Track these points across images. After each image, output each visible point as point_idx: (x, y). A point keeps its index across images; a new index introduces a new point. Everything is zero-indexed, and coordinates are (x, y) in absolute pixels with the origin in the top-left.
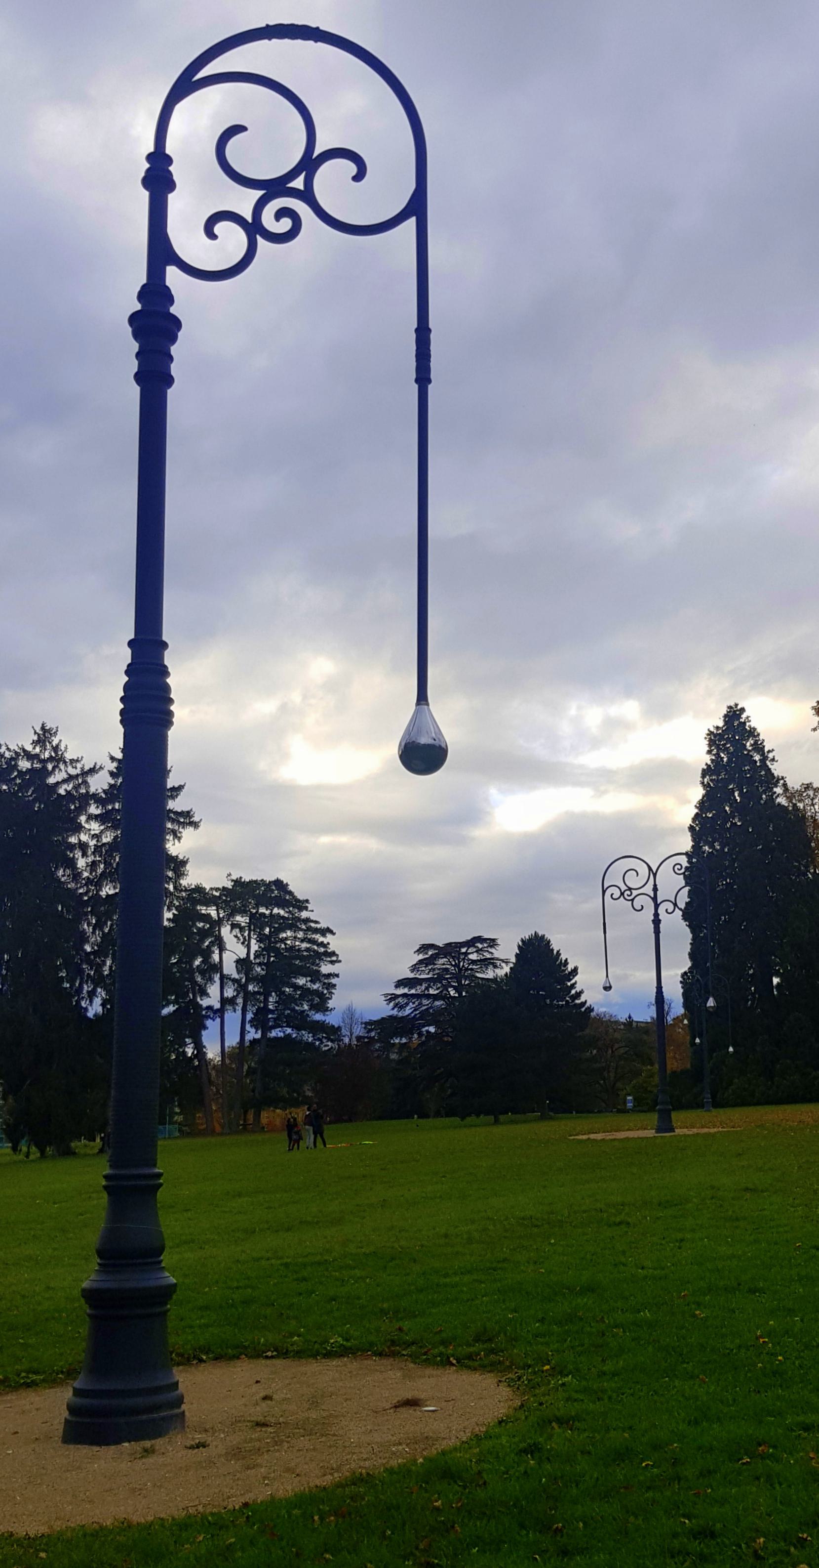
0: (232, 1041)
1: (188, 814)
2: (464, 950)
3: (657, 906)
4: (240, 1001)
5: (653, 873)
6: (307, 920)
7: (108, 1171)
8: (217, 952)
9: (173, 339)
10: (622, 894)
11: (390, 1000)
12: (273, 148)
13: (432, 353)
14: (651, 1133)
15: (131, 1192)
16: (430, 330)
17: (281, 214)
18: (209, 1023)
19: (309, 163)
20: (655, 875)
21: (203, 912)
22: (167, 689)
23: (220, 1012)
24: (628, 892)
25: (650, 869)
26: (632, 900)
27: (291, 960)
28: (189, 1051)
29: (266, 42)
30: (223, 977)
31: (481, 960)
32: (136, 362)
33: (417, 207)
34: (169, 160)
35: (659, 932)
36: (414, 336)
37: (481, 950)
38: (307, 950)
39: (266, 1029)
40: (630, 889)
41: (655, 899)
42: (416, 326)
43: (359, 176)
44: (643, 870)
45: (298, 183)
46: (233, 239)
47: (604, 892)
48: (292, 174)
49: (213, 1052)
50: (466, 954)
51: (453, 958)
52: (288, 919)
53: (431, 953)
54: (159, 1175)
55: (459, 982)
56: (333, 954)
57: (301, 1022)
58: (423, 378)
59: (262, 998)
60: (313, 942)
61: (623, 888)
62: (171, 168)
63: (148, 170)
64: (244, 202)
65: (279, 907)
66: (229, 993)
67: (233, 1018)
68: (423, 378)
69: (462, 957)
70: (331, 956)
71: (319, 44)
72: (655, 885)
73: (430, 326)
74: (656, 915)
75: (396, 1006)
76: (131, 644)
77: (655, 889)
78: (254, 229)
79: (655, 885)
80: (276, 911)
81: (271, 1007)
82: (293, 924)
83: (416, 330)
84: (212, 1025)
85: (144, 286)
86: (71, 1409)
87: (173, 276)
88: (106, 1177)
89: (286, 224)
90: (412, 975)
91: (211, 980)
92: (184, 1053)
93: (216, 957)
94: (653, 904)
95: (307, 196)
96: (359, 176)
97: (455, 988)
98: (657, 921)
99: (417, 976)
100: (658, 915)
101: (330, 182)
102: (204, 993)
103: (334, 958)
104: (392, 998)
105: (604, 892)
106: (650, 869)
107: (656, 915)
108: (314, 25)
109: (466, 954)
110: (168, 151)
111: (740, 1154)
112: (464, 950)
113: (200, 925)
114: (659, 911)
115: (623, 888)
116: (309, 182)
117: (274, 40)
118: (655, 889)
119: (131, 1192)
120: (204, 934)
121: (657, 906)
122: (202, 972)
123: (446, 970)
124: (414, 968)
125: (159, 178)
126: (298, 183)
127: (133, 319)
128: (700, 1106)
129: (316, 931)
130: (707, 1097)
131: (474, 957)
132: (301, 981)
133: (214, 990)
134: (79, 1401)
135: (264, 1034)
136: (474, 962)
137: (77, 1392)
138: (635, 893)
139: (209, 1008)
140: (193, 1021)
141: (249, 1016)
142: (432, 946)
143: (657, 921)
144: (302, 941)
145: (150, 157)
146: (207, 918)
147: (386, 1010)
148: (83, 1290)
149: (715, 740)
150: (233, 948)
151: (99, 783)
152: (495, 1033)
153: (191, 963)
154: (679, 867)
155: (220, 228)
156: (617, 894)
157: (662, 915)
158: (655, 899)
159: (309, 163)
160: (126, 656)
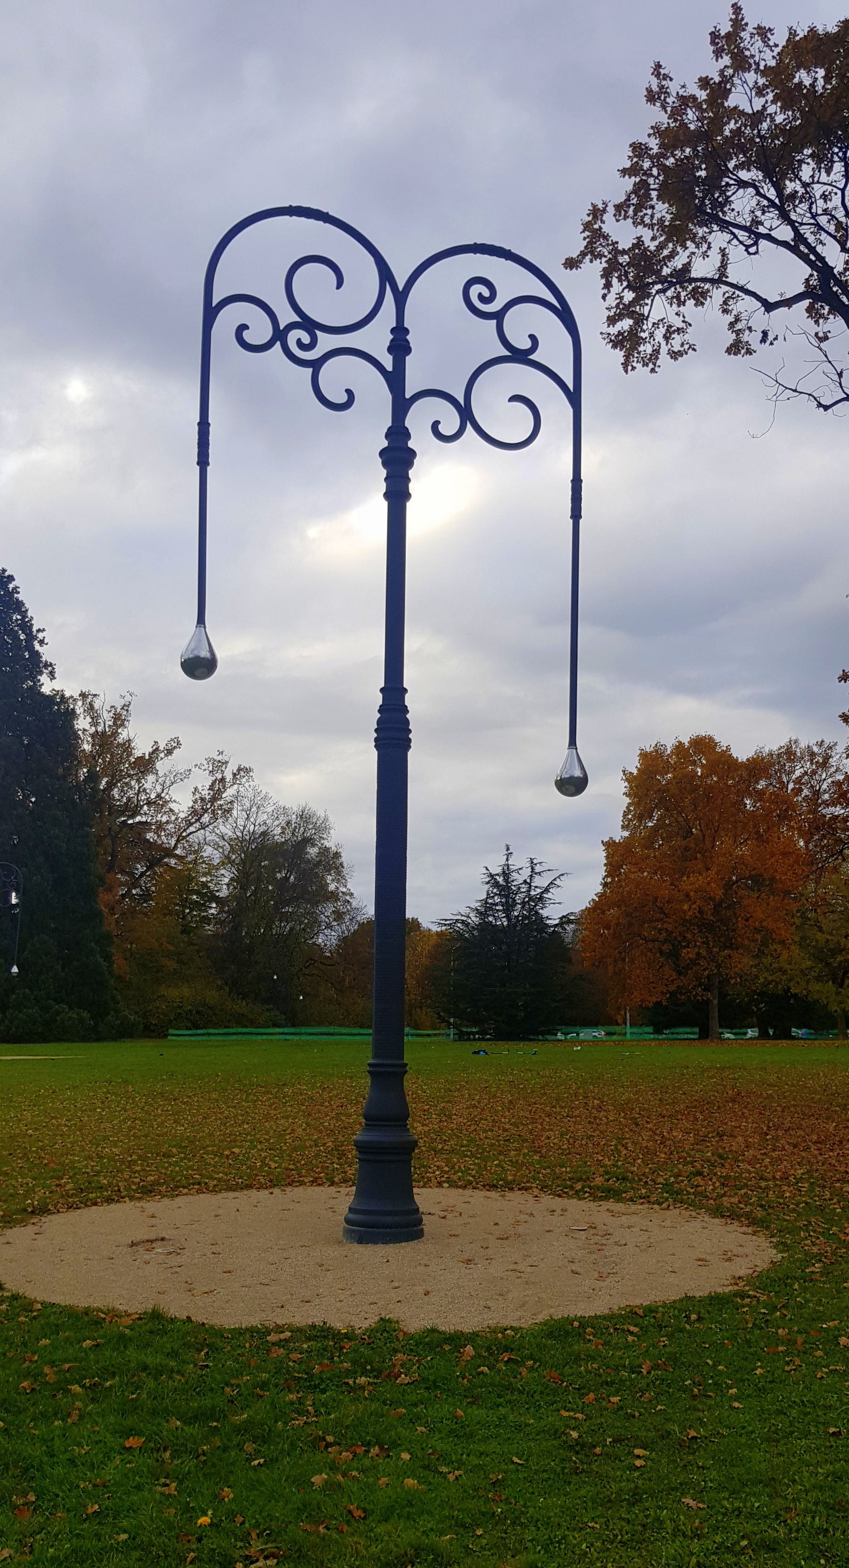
3: (401, 406)
5: (395, 289)
7: (371, 1061)
10: (280, 335)
13: (210, 442)
15: (388, 1074)
16: (209, 424)
20: (401, 299)
22: (407, 722)
26: (316, 365)
29: (287, 217)
32: (385, 484)
34: (407, 331)
35: (406, 495)
40: (308, 324)
41: (395, 379)
42: (198, 420)
47: (211, 313)
58: (576, 514)
61: (287, 316)
62: (408, 337)
63: (392, 341)
68: (576, 514)
71: (509, 262)
73: (210, 421)
76: (382, 690)
77: (400, 345)
79: (400, 332)
83: (572, 481)
85: (389, 429)
88: (370, 1065)
94: (388, 397)
100: (406, 435)
105: (211, 313)
110: (406, 326)
114: (410, 422)
115: (287, 316)
117: (478, 255)
118: (400, 345)
119: (388, 1074)
121: (401, 406)
127: (382, 453)
134: (351, 1216)
138: (326, 342)
145: (393, 331)
148: (355, 1141)
156: (260, 330)
157: (420, 439)
158: (395, 379)
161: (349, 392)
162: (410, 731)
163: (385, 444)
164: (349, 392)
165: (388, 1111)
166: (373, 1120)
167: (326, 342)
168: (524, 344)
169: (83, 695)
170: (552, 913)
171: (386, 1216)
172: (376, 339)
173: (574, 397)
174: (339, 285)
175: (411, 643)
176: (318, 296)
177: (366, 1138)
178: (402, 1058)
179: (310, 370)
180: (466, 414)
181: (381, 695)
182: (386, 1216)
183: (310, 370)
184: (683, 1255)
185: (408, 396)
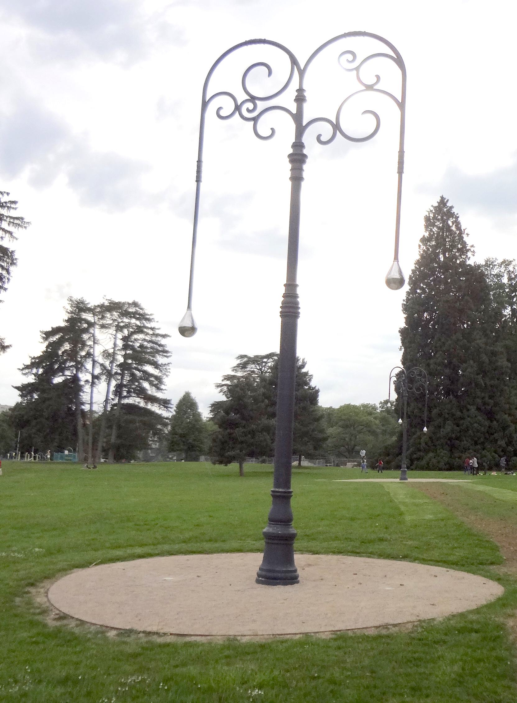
2: (265, 360)
3: (300, 130)
6: (152, 329)
10: (238, 108)
20: (302, 73)
24: (250, 106)
25: (294, 61)
26: (255, 120)
38: (152, 348)
39: (121, 397)
40: (253, 99)
41: (298, 117)
44: (281, 64)
47: (205, 104)
51: (258, 364)
54: (291, 492)
56: (167, 352)
57: (141, 392)
58: (199, 162)
59: (119, 377)
66: (97, 371)
68: (199, 162)
69: (264, 364)
72: (300, 91)
74: (298, 145)
77: (300, 99)
79: (300, 91)
81: (125, 383)
82: (140, 330)
88: (272, 491)
90: (233, 373)
98: (298, 158)
99: (236, 374)
105: (205, 104)
106: (294, 61)
107: (298, 145)
109: (266, 363)
112: (265, 360)
118: (300, 99)
119: (282, 497)
123: (253, 372)
124: (235, 369)
127: (290, 156)
129: (157, 335)
132: (149, 368)
141: (112, 388)
142: (246, 356)
143: (298, 158)
145: (297, 91)
149: (429, 222)
154: (350, 57)
155: (270, 132)
156: (228, 106)
157: (311, 148)
158: (298, 117)
162: (299, 308)
163: (291, 151)
165: (282, 517)
166: (273, 521)
168: (371, 81)
169: (46, 339)
171: (278, 572)
172: (288, 100)
173: (402, 105)
176: (260, 86)
177: (271, 530)
178: (289, 488)
179: (252, 123)
180: (336, 127)
181: (284, 288)
182: (278, 572)
183: (252, 123)
184: (438, 594)
185: (304, 125)
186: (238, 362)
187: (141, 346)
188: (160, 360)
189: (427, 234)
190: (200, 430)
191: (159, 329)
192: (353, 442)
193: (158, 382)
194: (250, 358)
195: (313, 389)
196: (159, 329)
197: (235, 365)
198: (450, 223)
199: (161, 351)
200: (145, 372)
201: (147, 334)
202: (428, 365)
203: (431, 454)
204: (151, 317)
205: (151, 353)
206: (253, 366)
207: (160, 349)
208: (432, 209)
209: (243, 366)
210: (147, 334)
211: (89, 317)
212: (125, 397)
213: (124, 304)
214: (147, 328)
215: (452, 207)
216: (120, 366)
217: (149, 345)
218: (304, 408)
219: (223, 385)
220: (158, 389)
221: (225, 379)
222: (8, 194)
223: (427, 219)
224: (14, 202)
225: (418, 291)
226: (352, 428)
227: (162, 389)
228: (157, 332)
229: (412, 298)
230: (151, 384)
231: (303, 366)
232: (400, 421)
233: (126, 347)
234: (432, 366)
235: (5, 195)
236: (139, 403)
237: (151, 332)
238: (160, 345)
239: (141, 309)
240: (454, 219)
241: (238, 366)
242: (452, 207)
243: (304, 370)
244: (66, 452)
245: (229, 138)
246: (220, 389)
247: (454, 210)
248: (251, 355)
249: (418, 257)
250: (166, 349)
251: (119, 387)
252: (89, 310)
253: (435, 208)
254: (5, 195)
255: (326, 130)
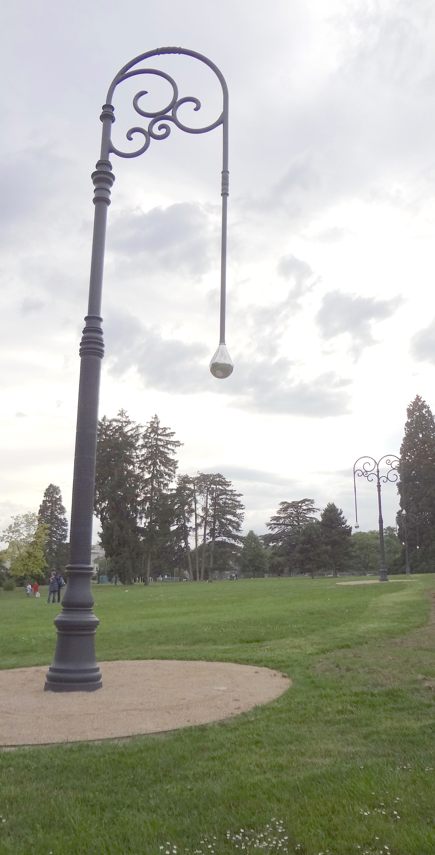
0: (200, 542)
1: (178, 442)
2: (300, 505)
4: (203, 524)
6: (231, 491)
8: (194, 503)
9: (111, 184)
10: (363, 474)
11: (268, 525)
12: (158, 100)
14: (378, 581)
17: (161, 127)
18: (190, 533)
19: (175, 105)
20: (378, 465)
21: (188, 487)
23: (196, 529)
25: (376, 462)
26: (368, 476)
27: (225, 507)
28: (183, 545)
30: (196, 515)
31: (308, 509)
33: (223, 120)
36: (221, 175)
37: (307, 504)
40: (366, 471)
41: (378, 476)
43: (197, 109)
45: (170, 114)
46: (139, 139)
47: (355, 473)
48: (167, 110)
49: (192, 546)
50: (301, 506)
52: (223, 490)
53: (286, 506)
55: (298, 519)
56: (242, 506)
57: (229, 534)
60: (234, 500)
64: (144, 123)
65: (220, 485)
66: (199, 521)
67: (201, 531)
70: (240, 506)
72: (378, 469)
74: (379, 483)
75: (270, 528)
77: (378, 471)
78: (149, 134)
79: (378, 469)
80: (218, 487)
84: (192, 533)
86: (49, 678)
87: (112, 158)
89: (163, 131)
90: (278, 515)
91: (191, 516)
92: (181, 546)
93: (193, 506)
95: (173, 119)
96: (197, 109)
97: (296, 521)
98: (379, 486)
101: (185, 113)
102: (189, 521)
103: (243, 507)
104: (268, 525)
105: (355, 473)
106: (376, 462)
107: (379, 483)
108: (178, 47)
109: (301, 506)
111: (412, 587)
112: (300, 505)
113: (187, 492)
115: (363, 471)
116: (174, 114)
118: (378, 471)
120: (189, 496)
122: (188, 513)
123: (292, 513)
124: (279, 512)
125: (108, 116)
126: (170, 114)
128: (404, 573)
129: (235, 495)
130: (408, 569)
131: (305, 508)
132: (229, 517)
133: (193, 519)
135: (213, 539)
136: (304, 510)
137: (51, 669)
138: (369, 473)
139: (191, 528)
140: (183, 533)
141: (208, 531)
143: (379, 486)
144: (229, 500)
145: (104, 107)
146: (189, 489)
147: (267, 531)
149: (410, 413)
150: (201, 502)
151: (142, 431)
152: (315, 543)
153: (183, 508)
154: (389, 461)
155: (134, 135)
156: (361, 474)
158: (378, 476)
159: (175, 105)
160: (83, 324)
161: (130, 139)
164: (130, 139)
167: (369, 473)
170: (100, 541)
174: (143, 93)
175: (109, 259)
176: (368, 468)
180: (387, 478)
186: (281, 507)
187: (225, 503)
188: (239, 511)
189: (409, 421)
190: (262, 556)
191: (235, 491)
192: (367, 560)
193: (237, 526)
194: (289, 503)
195: (348, 527)
196: (235, 491)
197: (278, 510)
198: (424, 412)
199: (238, 505)
200: (227, 519)
201: (228, 494)
202: (418, 506)
203: (424, 563)
204: (229, 484)
205: (231, 507)
206: (290, 509)
207: (237, 504)
208: (411, 403)
209: (285, 510)
210: (228, 494)
211: (191, 486)
212: (217, 537)
213: (211, 475)
214: (228, 491)
215: (424, 401)
216: (213, 516)
217: (230, 502)
218: (344, 539)
219: (272, 524)
220: (238, 530)
221: (272, 520)
222: (170, 428)
223: (408, 410)
224: (174, 433)
225: (407, 458)
226: (366, 550)
227: (240, 530)
228: (234, 493)
229: (403, 463)
230: (234, 527)
231: (341, 513)
232: (403, 543)
233: (214, 504)
234: (420, 507)
235: (168, 429)
236: (225, 540)
237: (230, 493)
238: (237, 501)
239: (224, 479)
240: (427, 409)
241: (281, 510)
242: (424, 401)
243: (342, 516)
244: (166, 577)
245: (362, 482)
246: (269, 527)
247: (426, 403)
248: (290, 501)
249: (405, 436)
250: (241, 504)
251: (212, 531)
252: (189, 482)
253: (414, 403)
254: (168, 429)
255: (385, 479)
